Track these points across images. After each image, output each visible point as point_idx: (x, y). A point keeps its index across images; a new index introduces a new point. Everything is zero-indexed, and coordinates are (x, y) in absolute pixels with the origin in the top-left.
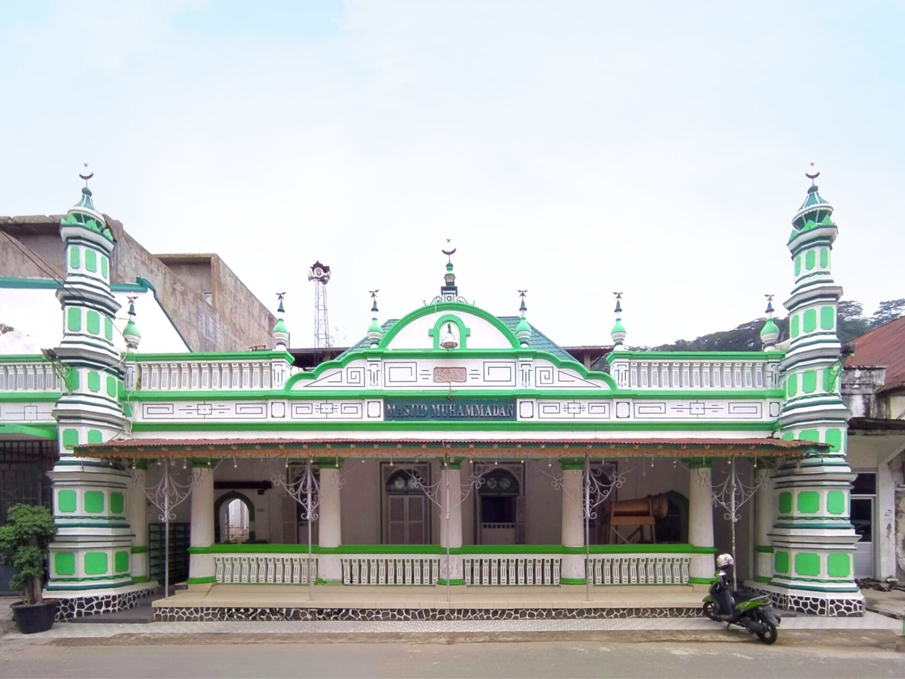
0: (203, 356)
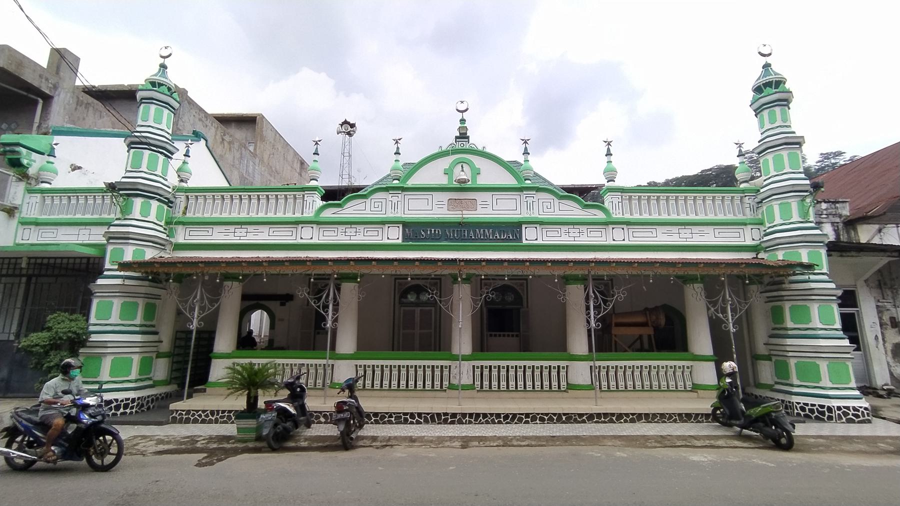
0: (240, 190)
